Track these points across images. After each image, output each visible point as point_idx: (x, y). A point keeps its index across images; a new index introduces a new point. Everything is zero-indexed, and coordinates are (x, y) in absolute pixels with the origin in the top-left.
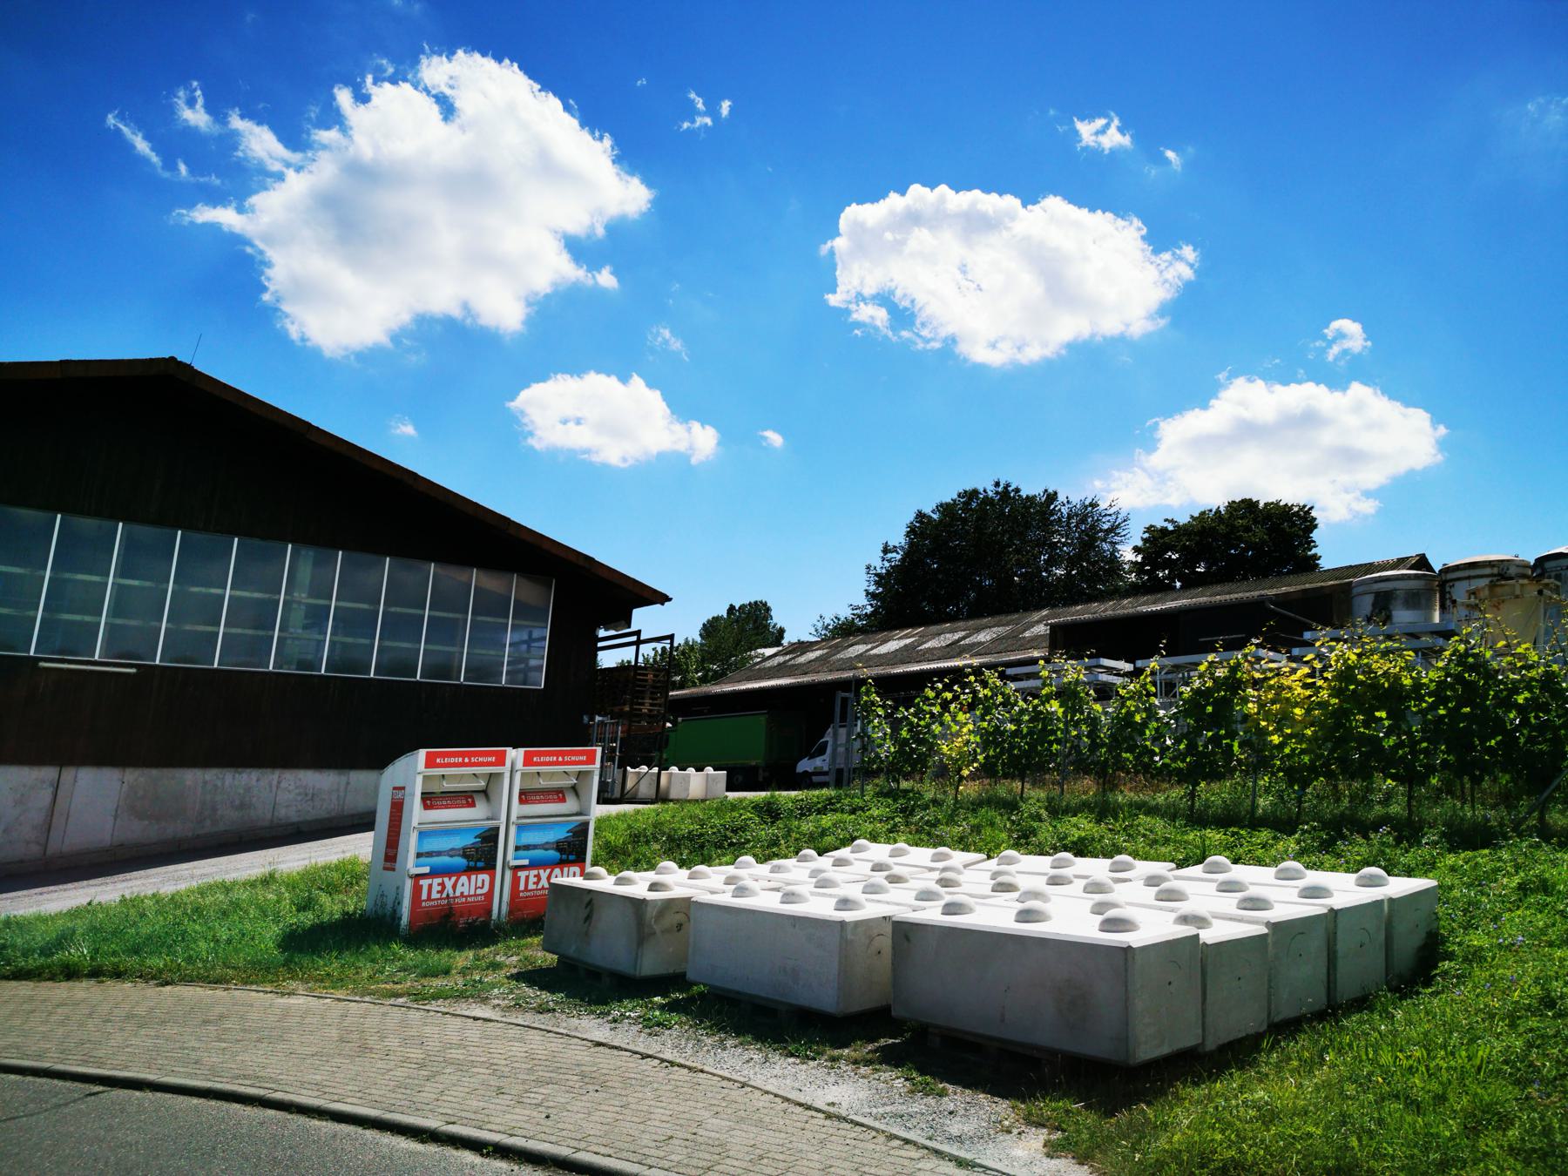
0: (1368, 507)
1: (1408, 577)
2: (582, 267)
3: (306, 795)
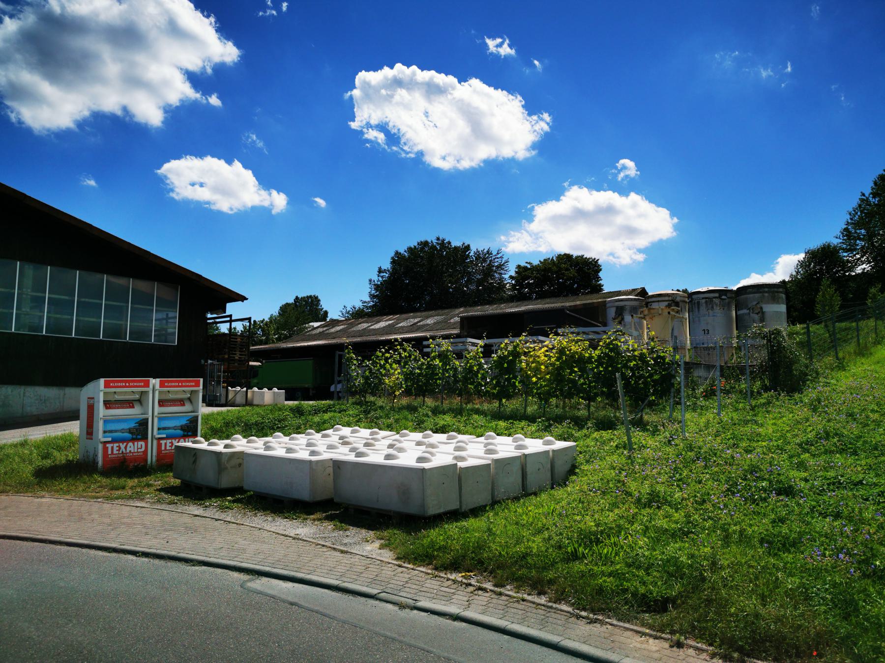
0: (640, 257)
1: (631, 299)
2: (199, 92)
3: (41, 400)
